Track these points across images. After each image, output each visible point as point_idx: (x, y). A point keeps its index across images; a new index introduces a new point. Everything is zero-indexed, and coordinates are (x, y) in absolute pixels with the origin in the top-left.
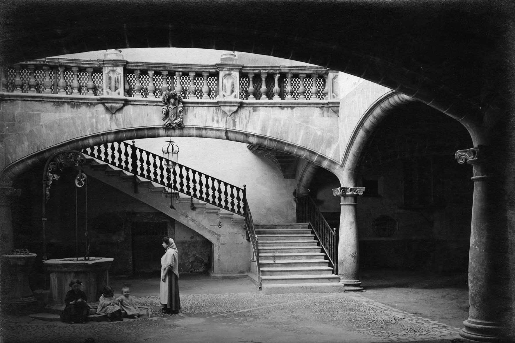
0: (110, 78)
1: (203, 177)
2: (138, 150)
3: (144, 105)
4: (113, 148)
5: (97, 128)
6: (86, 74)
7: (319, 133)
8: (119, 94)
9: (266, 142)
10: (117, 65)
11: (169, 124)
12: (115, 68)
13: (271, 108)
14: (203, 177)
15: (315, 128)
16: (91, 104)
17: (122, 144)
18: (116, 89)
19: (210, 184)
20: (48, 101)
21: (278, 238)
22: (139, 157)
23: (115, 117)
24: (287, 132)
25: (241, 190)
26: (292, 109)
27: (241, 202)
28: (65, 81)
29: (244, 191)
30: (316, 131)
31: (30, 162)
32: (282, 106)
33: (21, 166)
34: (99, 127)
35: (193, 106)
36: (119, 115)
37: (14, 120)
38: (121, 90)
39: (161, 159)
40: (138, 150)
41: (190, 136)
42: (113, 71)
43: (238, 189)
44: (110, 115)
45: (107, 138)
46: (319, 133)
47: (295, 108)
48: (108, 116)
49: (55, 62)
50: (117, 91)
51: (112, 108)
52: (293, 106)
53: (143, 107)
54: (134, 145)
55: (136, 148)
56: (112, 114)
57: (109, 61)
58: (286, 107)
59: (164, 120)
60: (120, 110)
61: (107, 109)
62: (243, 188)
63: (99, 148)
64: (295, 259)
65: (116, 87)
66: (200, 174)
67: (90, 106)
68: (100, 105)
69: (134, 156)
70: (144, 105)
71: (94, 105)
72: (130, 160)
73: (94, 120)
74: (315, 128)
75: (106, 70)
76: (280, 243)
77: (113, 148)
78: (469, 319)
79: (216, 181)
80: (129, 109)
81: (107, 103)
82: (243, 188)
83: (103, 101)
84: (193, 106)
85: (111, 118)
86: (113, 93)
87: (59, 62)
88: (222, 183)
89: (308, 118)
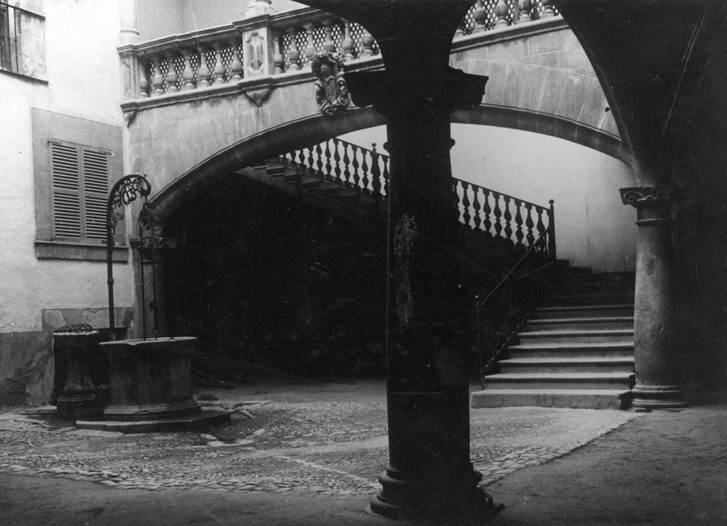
0: (252, 48)
1: (481, 193)
2: (380, 157)
4: (319, 151)
5: (240, 132)
6: (230, 49)
7: (576, 81)
8: (262, 71)
10: (258, 26)
11: (328, 108)
12: (256, 31)
13: (487, 48)
14: (481, 193)
15: (570, 71)
16: (232, 95)
18: (260, 64)
19: (482, 202)
23: (262, 110)
24: (516, 90)
25: (545, 211)
27: (369, 173)
28: (176, 73)
29: (551, 213)
30: (571, 77)
31: (171, 197)
33: (164, 204)
34: (243, 130)
36: (267, 107)
37: (150, 139)
38: (266, 65)
39: (364, 151)
40: (380, 157)
42: (255, 35)
43: (540, 209)
46: (576, 81)
47: (530, 38)
53: (296, 86)
54: (374, 150)
55: (378, 155)
60: (266, 98)
61: (252, 101)
62: (548, 206)
63: (302, 152)
65: (259, 61)
66: (475, 188)
67: (231, 100)
68: (242, 96)
72: (370, 177)
73: (237, 121)
74: (570, 71)
75: (246, 36)
77: (319, 151)
78: (636, 386)
79: (512, 202)
80: (280, 93)
82: (548, 206)
85: (257, 113)
86: (257, 72)
89: (553, 55)
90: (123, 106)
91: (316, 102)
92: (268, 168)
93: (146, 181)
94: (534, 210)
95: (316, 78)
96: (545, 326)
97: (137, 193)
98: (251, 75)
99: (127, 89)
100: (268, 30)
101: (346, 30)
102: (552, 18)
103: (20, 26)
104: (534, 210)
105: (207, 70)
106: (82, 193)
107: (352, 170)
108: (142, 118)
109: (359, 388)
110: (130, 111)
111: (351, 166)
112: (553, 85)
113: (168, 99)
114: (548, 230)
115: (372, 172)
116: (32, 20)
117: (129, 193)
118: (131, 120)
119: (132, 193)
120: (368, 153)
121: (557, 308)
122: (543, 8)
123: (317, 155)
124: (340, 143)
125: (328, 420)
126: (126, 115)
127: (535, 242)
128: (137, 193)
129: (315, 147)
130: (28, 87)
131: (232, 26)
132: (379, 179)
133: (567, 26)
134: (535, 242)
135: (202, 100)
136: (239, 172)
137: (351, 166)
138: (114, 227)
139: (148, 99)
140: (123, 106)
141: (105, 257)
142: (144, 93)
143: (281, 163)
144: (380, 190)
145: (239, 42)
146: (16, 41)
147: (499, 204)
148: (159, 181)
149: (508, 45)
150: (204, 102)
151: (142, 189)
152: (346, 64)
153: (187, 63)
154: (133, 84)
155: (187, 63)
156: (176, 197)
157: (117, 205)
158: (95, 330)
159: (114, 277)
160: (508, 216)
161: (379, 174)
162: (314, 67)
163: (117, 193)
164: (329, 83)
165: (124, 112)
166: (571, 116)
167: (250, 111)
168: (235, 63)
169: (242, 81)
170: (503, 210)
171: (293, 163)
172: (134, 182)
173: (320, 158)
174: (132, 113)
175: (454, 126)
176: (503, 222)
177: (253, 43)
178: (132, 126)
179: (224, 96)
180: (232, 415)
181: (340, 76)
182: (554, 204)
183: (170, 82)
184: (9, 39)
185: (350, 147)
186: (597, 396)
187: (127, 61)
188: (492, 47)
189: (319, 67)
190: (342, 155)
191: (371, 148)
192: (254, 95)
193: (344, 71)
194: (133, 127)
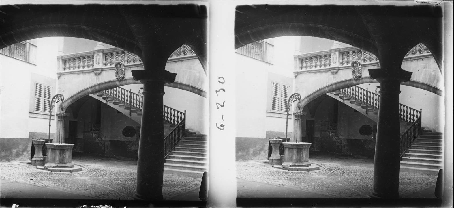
0: (97, 59)
3: (346, 69)
4: (114, 90)
9: (339, 85)
10: (99, 52)
12: (335, 53)
16: (327, 71)
17: (120, 88)
20: (312, 72)
21: (193, 143)
22: (369, 96)
25: (183, 114)
26: (417, 61)
32: (176, 60)
35: (131, 68)
39: (364, 90)
41: (131, 84)
42: (335, 54)
43: (181, 113)
44: (333, 75)
45: (96, 88)
48: (96, 77)
49: (78, 55)
50: (336, 63)
51: (97, 73)
52: (182, 60)
54: (367, 90)
56: (334, 75)
57: (96, 51)
58: (179, 61)
59: (353, 75)
61: (96, 74)
62: (184, 112)
64: (195, 156)
69: (367, 94)
70: (346, 69)
71: (90, 72)
76: (195, 146)
81: (95, 71)
83: (330, 69)
84: (367, 66)
85: (97, 78)
86: (98, 66)
87: (80, 55)
88: (173, 110)
90: (57, 73)
91: (115, 76)
92: (98, 94)
93: (63, 96)
94: (179, 113)
95: (115, 68)
96: (181, 150)
97: (60, 100)
98: (332, 66)
99: (58, 69)
100: (102, 54)
101: (126, 55)
102: (426, 54)
103: (267, 48)
104: (179, 113)
105: (83, 64)
106: (43, 98)
107: (360, 96)
108: (62, 77)
109: (348, 163)
110: (296, 74)
111: (360, 94)
112: (425, 74)
113: (70, 72)
114: (183, 120)
115: (129, 98)
116: (271, 46)
117: (295, 99)
118: (59, 77)
119: (58, 99)
120: (365, 90)
121: (421, 142)
122: (188, 52)
123: (350, 90)
124: (120, 88)
125: (112, 173)
126: (295, 75)
127: (415, 121)
128: (60, 100)
129: (344, 89)
130: (268, 65)
131: (91, 52)
132: (131, 100)
133: (432, 56)
134: (415, 121)
135: (317, 72)
136: (89, 95)
137: (360, 94)
138: (52, 109)
139: (64, 72)
140: (57, 73)
141: (49, 118)
142: (63, 70)
143: (339, 92)
144: (368, 102)
145: (93, 57)
146: (28, 53)
147: (408, 110)
148: (304, 95)
149: (177, 63)
150: (81, 74)
151: (61, 99)
152: (125, 65)
153: (314, 61)
154: (60, 67)
155: (314, 61)
156: (307, 100)
157: (54, 103)
158: (282, 138)
159: (288, 123)
160: (407, 113)
161: (368, 97)
162: (115, 65)
163: (54, 99)
164: (356, 69)
165: (294, 74)
166: (431, 84)
167: (332, 76)
168: (91, 63)
169: (330, 67)
170: (405, 111)
171: (106, 93)
172: (59, 96)
173: (114, 92)
174: (296, 74)
175: (401, 85)
176: (405, 114)
177: (334, 56)
178: (296, 78)
179: (87, 72)
180: (83, 169)
181: (123, 69)
182: (186, 112)
183: (304, 67)
184: (263, 52)
185: (362, 89)
186: (433, 171)
187: (296, 59)
188: (407, 61)
189: (117, 65)
190: (120, 92)
191: (366, 89)
192: (333, 72)
193: (125, 67)
194: (60, 80)
